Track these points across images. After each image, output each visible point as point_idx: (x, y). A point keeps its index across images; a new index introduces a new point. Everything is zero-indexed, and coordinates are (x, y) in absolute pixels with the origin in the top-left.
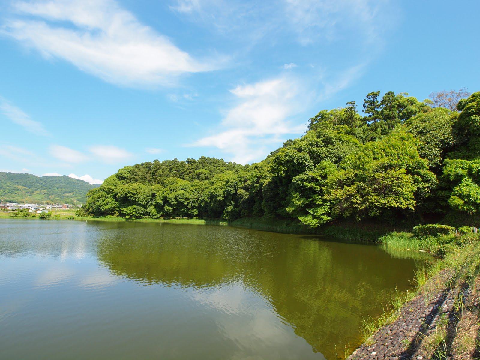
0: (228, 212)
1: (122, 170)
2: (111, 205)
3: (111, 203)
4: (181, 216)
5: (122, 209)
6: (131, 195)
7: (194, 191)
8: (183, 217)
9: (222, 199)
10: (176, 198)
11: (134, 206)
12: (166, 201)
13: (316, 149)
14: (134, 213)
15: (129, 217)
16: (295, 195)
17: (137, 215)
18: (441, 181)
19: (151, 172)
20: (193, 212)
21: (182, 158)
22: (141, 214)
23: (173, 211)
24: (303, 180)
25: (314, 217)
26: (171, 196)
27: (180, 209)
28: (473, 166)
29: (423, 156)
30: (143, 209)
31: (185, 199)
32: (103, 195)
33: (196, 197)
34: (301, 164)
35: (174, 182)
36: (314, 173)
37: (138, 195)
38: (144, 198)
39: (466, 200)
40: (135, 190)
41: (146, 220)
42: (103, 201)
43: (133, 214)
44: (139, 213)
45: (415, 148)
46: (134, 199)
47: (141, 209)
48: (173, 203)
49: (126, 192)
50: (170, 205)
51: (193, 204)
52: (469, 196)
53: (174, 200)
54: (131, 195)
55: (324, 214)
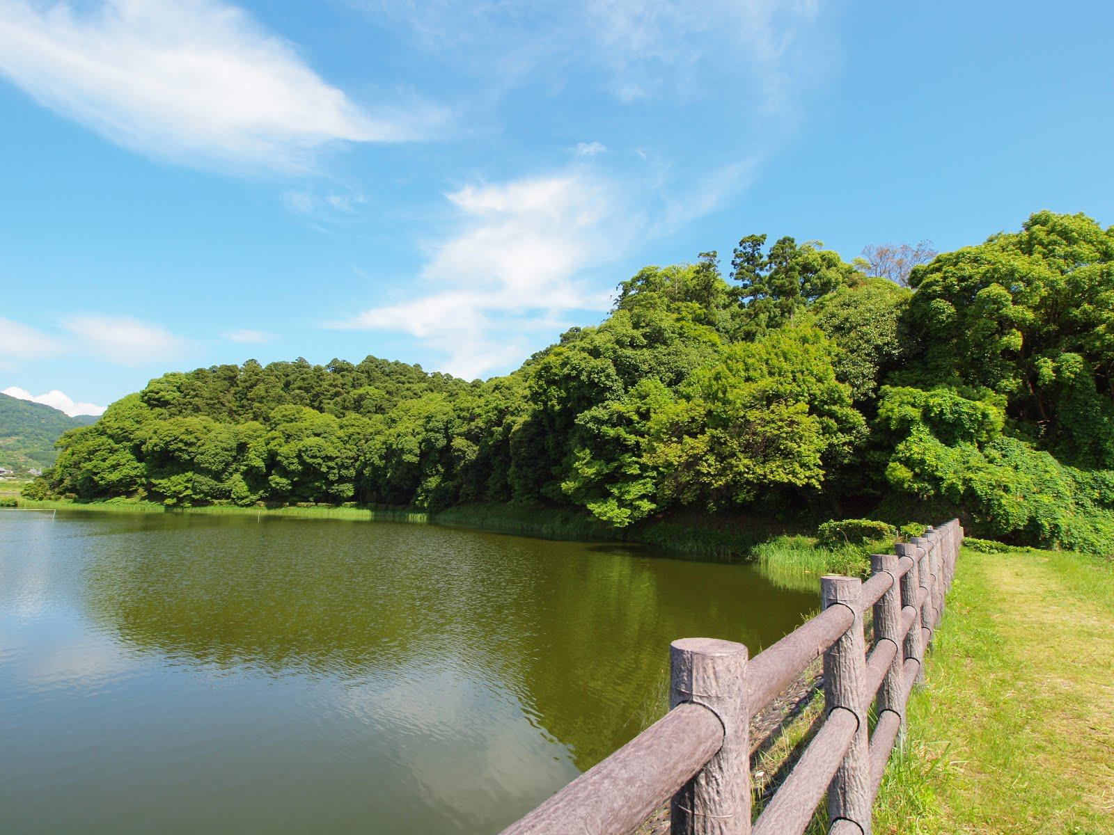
0: (428, 491)
1: (159, 382)
2: (125, 471)
3: (124, 465)
4: (311, 499)
5: (157, 482)
6: (180, 445)
7: (346, 438)
8: (317, 501)
9: (415, 459)
10: (299, 456)
11: (190, 474)
12: (273, 461)
13: (629, 352)
14: (189, 492)
15: (175, 500)
17: (196, 497)
18: (874, 429)
19: (236, 390)
20: (343, 491)
21: (319, 359)
22: (206, 494)
23: (290, 487)
24: (596, 420)
25: (622, 503)
26: (286, 450)
27: (310, 482)
28: (931, 401)
29: (842, 378)
30: (213, 483)
31: (322, 458)
32: (103, 444)
33: (350, 454)
34: (597, 385)
35: (297, 416)
36: (623, 405)
37: (199, 446)
39: (917, 470)
40: (191, 433)
41: (217, 509)
42: (104, 460)
43: (185, 494)
44: (202, 492)
45: (828, 359)
47: (206, 482)
48: (292, 467)
49: (168, 439)
50: (285, 473)
51: (343, 472)
52: (922, 462)
53: (296, 460)
54: (180, 445)
55: (642, 497)
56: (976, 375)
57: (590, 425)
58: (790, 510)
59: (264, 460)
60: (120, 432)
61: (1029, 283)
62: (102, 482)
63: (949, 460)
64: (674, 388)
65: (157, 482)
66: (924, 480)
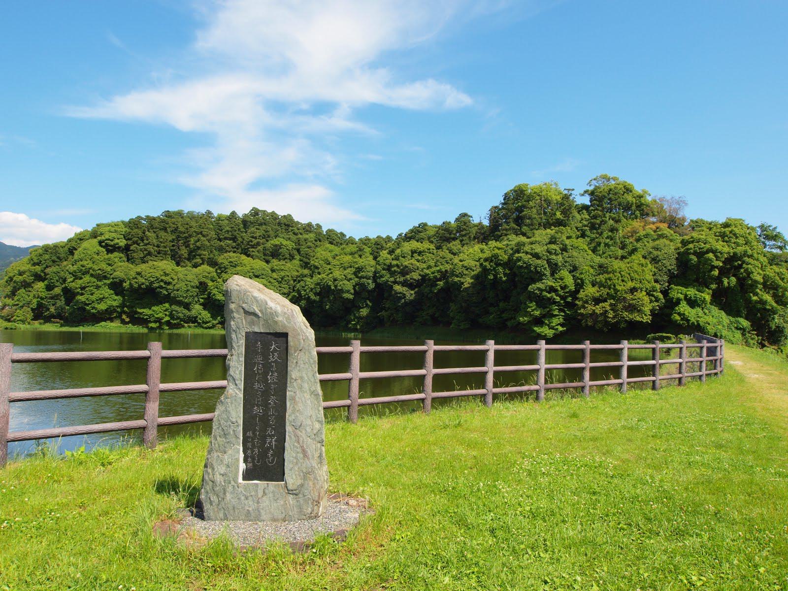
3: (107, 298)
6: (162, 284)
9: (351, 297)
13: (554, 257)
16: (531, 305)
18: (667, 301)
22: (181, 320)
24: (539, 289)
28: (688, 293)
29: (656, 281)
30: (185, 311)
34: (538, 272)
36: (549, 282)
38: (188, 290)
42: (92, 294)
44: (178, 318)
46: (167, 292)
49: (152, 280)
52: (684, 314)
54: (162, 284)
55: (559, 324)
56: (702, 282)
58: (635, 331)
60: (101, 273)
61: (721, 254)
62: (94, 311)
63: (692, 314)
64: (572, 274)
66: (684, 320)
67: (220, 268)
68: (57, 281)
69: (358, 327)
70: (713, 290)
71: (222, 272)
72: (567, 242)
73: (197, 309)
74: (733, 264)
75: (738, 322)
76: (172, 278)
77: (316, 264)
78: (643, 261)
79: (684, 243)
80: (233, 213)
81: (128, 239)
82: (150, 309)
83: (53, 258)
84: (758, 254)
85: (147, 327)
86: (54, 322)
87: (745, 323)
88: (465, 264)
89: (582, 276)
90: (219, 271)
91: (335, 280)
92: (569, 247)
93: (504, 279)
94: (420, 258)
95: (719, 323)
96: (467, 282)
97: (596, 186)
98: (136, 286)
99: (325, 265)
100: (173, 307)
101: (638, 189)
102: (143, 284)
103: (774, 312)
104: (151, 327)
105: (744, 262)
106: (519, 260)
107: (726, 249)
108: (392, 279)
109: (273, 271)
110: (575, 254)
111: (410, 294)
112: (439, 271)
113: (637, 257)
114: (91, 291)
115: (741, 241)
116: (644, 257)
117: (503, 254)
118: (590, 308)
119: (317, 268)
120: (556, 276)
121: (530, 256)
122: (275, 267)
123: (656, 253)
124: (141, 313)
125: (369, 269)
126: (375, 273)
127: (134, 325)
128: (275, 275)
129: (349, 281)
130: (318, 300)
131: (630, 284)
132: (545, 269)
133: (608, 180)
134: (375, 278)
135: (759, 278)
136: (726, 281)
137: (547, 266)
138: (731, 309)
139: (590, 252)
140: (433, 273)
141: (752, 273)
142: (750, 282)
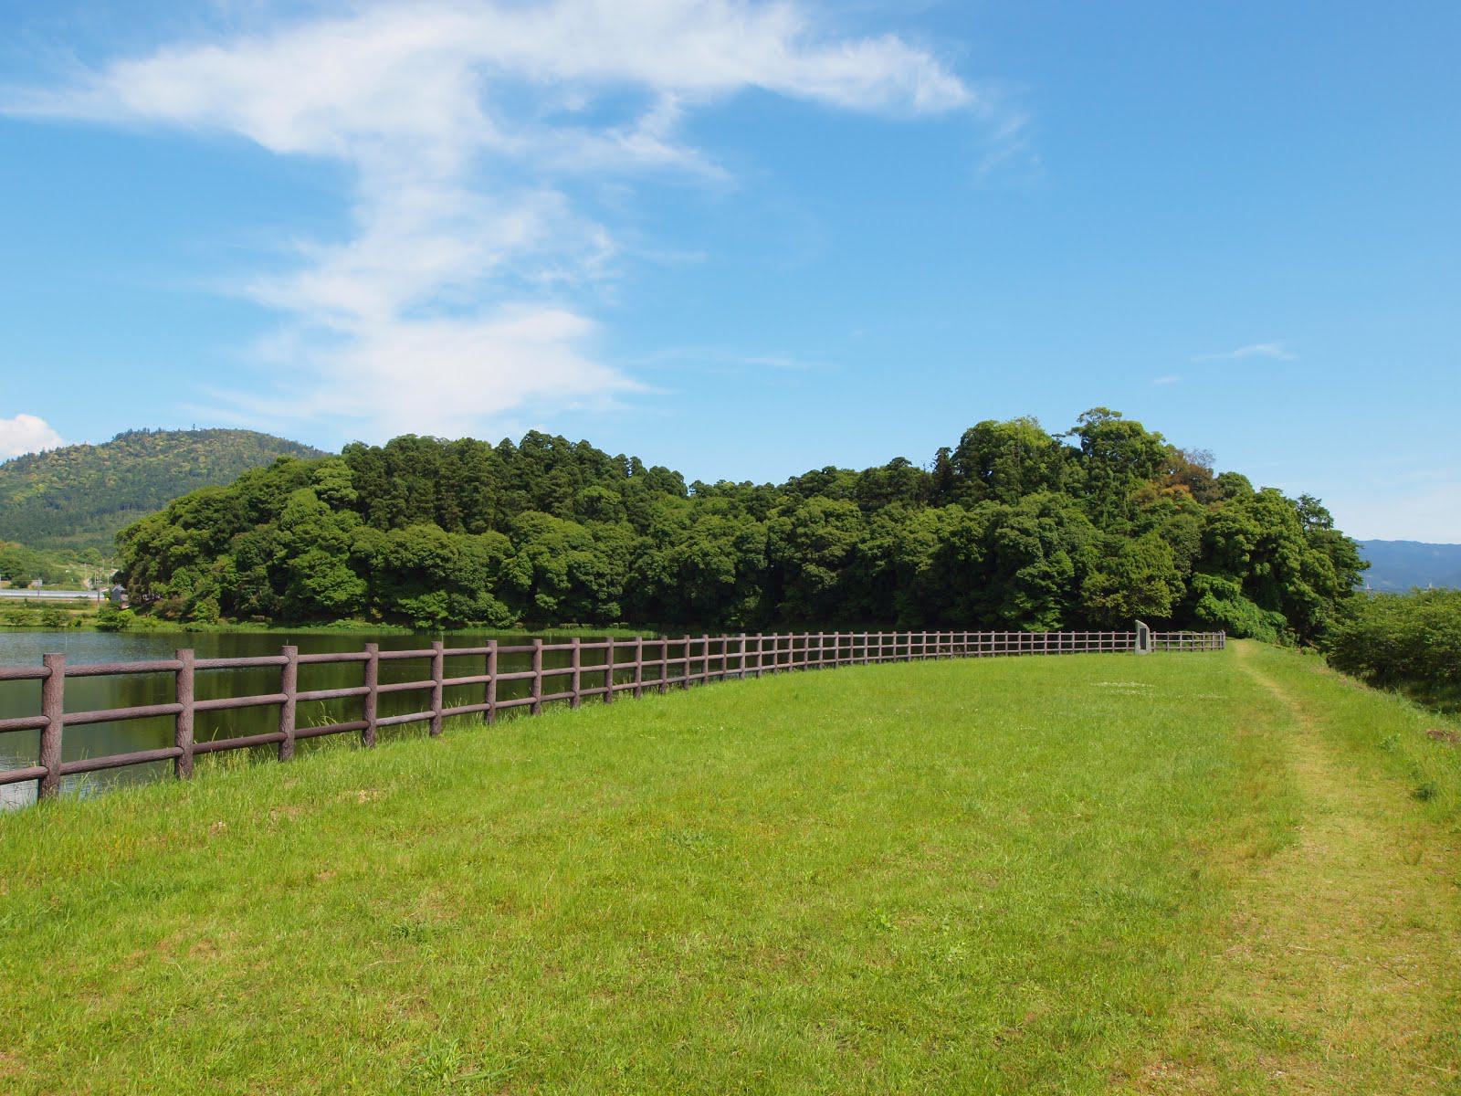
0: (745, 612)
4: (574, 620)
5: (404, 602)
6: (438, 561)
9: (732, 580)
13: (1048, 534)
22: (466, 616)
24: (1031, 575)
26: (557, 565)
29: (1177, 567)
30: (472, 603)
36: (1042, 565)
38: (475, 570)
44: (461, 612)
48: (562, 585)
50: (551, 589)
51: (612, 589)
53: (565, 578)
54: (438, 561)
55: (1054, 620)
56: (1231, 569)
57: (1027, 578)
59: (529, 577)
61: (1253, 535)
65: (404, 602)
67: (517, 535)
68: (257, 555)
69: (742, 625)
70: (1244, 579)
71: (521, 540)
72: (1063, 513)
73: (485, 598)
74: (1267, 547)
75: (1271, 616)
76: (452, 552)
77: (666, 528)
78: (1161, 542)
79: (1210, 520)
80: (506, 442)
81: (363, 488)
82: (416, 599)
83: (227, 517)
84: (1295, 535)
85: (413, 628)
86: (257, 621)
87: (1280, 618)
88: (919, 536)
89: (1084, 559)
90: (515, 540)
91: (706, 554)
92: (1066, 520)
93: (980, 560)
94: (839, 524)
95: (1250, 618)
96: (924, 563)
97: (1089, 423)
98: (398, 563)
99: (680, 531)
100: (454, 596)
101: (1149, 429)
102: (410, 560)
103: (1314, 604)
104: (421, 628)
105: (1279, 545)
106: (1004, 538)
107: (1258, 530)
108: (798, 555)
109: (597, 538)
110: (1073, 528)
111: (830, 577)
112: (879, 547)
113: (1152, 536)
114: (322, 571)
115: (1276, 519)
116: (1162, 537)
117: (976, 527)
118: (1099, 600)
119: (666, 534)
120: (1052, 558)
121: (1017, 533)
122: (600, 533)
123: (1176, 531)
124: (403, 606)
125: (759, 538)
126: (768, 544)
127: (390, 623)
128: (601, 546)
129: (727, 556)
130: (675, 584)
131: (1146, 572)
132: (1038, 549)
133: (1107, 414)
134: (768, 553)
135: (1296, 565)
136: (1258, 568)
137: (1040, 545)
138: (1264, 602)
139: (1091, 525)
140: (870, 549)
141: (1288, 558)
142: (1285, 569)
